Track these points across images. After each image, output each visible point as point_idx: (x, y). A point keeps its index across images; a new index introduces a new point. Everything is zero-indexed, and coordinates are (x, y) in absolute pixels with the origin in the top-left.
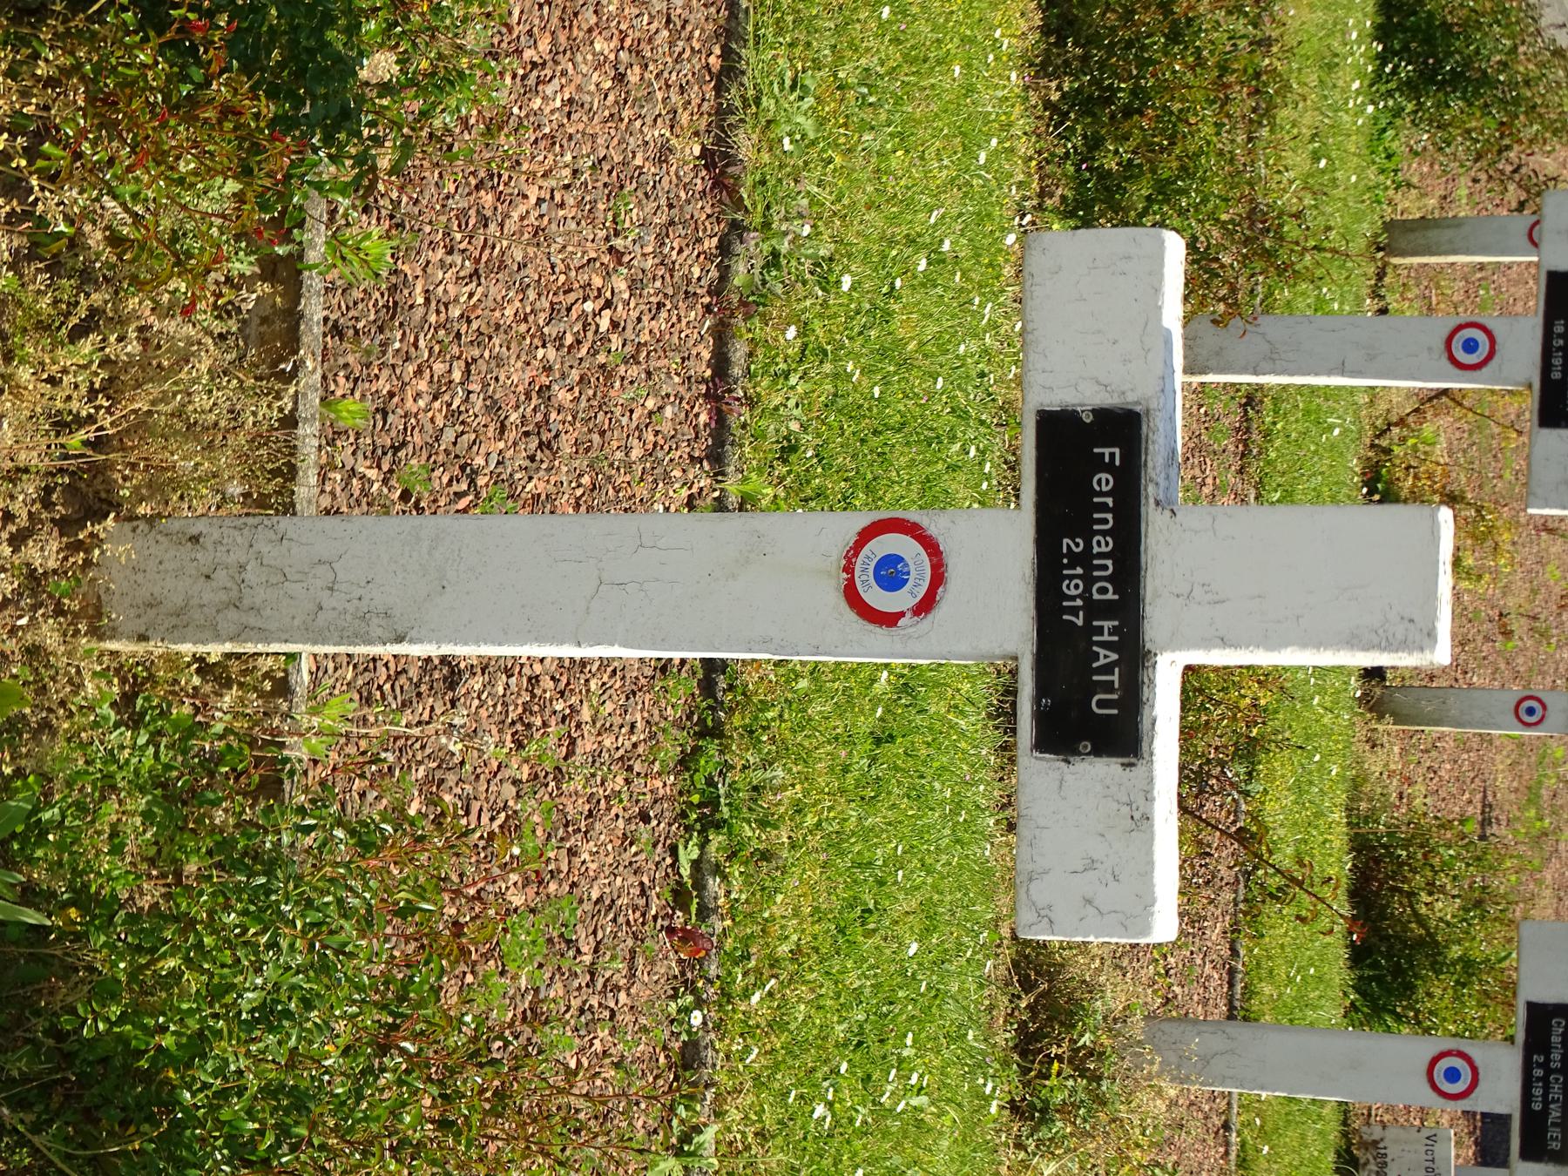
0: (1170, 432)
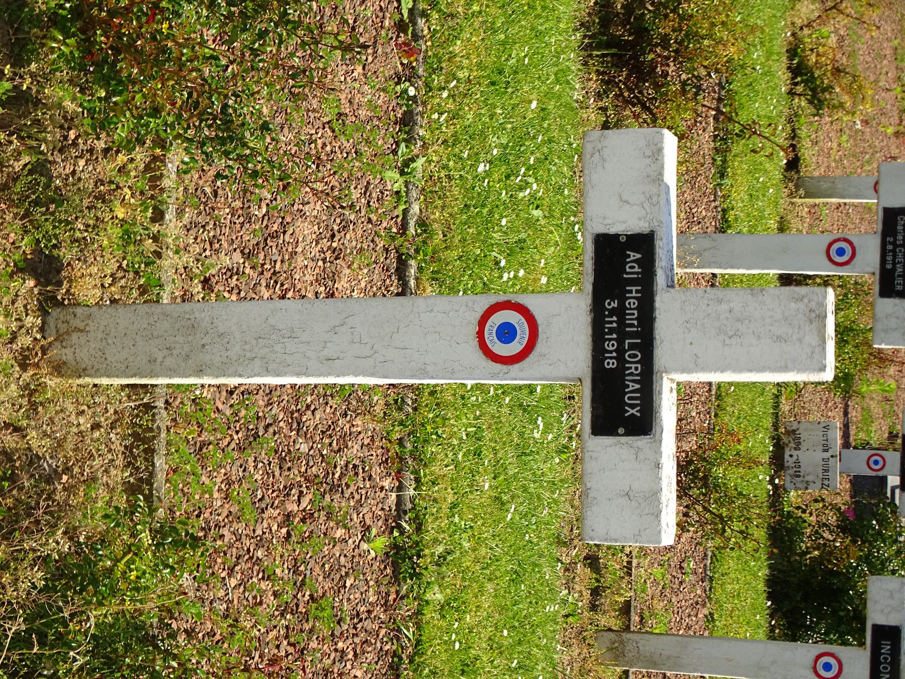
0: (669, 247)
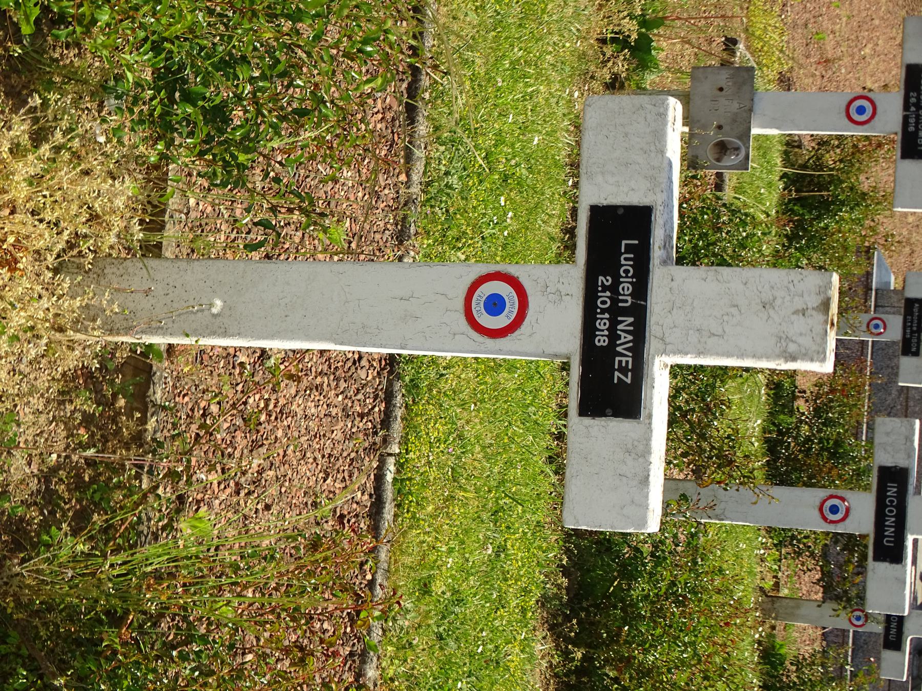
0: (666, 228)
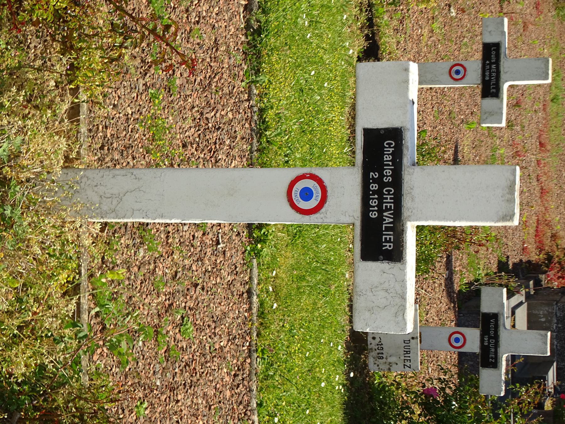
0: (411, 140)
